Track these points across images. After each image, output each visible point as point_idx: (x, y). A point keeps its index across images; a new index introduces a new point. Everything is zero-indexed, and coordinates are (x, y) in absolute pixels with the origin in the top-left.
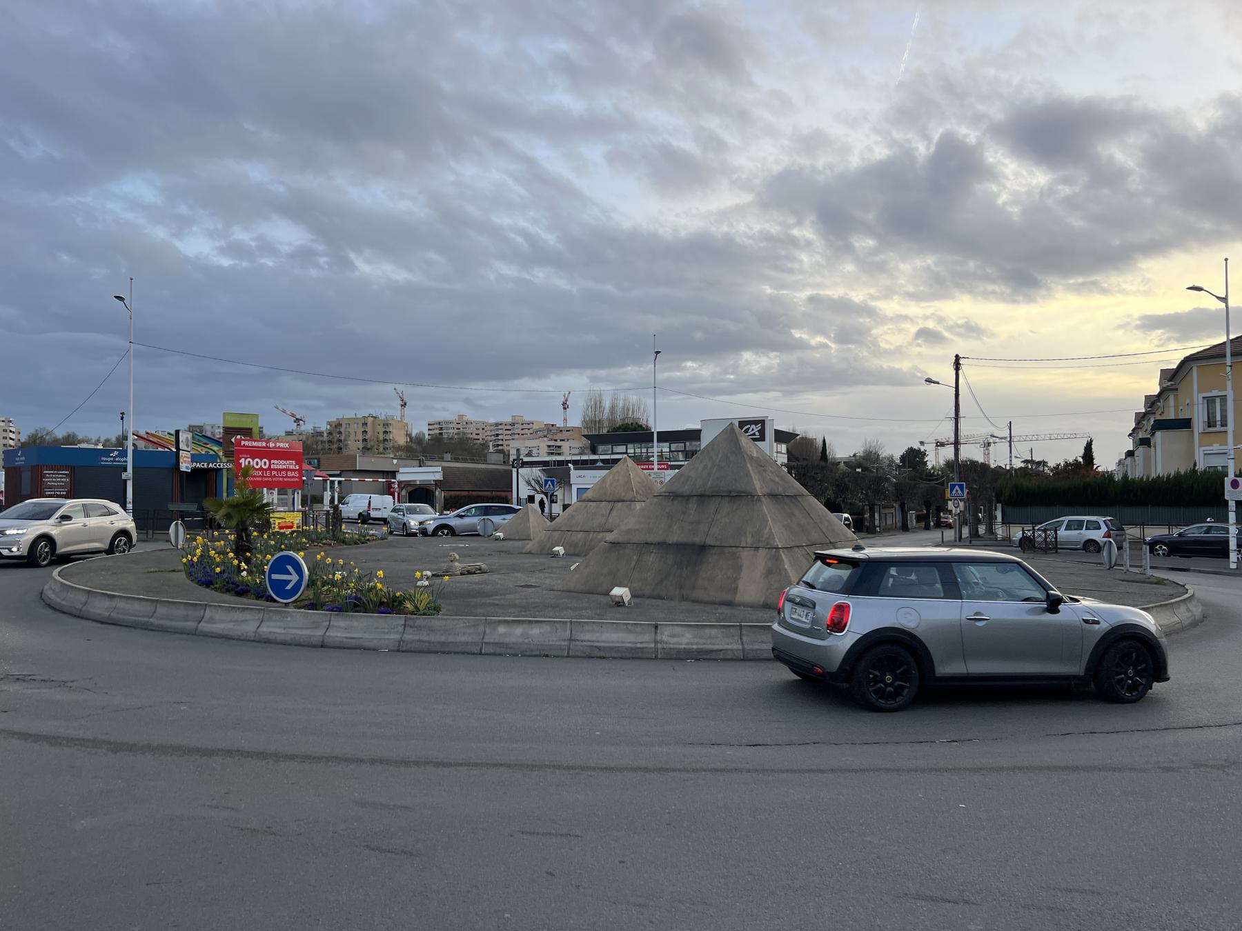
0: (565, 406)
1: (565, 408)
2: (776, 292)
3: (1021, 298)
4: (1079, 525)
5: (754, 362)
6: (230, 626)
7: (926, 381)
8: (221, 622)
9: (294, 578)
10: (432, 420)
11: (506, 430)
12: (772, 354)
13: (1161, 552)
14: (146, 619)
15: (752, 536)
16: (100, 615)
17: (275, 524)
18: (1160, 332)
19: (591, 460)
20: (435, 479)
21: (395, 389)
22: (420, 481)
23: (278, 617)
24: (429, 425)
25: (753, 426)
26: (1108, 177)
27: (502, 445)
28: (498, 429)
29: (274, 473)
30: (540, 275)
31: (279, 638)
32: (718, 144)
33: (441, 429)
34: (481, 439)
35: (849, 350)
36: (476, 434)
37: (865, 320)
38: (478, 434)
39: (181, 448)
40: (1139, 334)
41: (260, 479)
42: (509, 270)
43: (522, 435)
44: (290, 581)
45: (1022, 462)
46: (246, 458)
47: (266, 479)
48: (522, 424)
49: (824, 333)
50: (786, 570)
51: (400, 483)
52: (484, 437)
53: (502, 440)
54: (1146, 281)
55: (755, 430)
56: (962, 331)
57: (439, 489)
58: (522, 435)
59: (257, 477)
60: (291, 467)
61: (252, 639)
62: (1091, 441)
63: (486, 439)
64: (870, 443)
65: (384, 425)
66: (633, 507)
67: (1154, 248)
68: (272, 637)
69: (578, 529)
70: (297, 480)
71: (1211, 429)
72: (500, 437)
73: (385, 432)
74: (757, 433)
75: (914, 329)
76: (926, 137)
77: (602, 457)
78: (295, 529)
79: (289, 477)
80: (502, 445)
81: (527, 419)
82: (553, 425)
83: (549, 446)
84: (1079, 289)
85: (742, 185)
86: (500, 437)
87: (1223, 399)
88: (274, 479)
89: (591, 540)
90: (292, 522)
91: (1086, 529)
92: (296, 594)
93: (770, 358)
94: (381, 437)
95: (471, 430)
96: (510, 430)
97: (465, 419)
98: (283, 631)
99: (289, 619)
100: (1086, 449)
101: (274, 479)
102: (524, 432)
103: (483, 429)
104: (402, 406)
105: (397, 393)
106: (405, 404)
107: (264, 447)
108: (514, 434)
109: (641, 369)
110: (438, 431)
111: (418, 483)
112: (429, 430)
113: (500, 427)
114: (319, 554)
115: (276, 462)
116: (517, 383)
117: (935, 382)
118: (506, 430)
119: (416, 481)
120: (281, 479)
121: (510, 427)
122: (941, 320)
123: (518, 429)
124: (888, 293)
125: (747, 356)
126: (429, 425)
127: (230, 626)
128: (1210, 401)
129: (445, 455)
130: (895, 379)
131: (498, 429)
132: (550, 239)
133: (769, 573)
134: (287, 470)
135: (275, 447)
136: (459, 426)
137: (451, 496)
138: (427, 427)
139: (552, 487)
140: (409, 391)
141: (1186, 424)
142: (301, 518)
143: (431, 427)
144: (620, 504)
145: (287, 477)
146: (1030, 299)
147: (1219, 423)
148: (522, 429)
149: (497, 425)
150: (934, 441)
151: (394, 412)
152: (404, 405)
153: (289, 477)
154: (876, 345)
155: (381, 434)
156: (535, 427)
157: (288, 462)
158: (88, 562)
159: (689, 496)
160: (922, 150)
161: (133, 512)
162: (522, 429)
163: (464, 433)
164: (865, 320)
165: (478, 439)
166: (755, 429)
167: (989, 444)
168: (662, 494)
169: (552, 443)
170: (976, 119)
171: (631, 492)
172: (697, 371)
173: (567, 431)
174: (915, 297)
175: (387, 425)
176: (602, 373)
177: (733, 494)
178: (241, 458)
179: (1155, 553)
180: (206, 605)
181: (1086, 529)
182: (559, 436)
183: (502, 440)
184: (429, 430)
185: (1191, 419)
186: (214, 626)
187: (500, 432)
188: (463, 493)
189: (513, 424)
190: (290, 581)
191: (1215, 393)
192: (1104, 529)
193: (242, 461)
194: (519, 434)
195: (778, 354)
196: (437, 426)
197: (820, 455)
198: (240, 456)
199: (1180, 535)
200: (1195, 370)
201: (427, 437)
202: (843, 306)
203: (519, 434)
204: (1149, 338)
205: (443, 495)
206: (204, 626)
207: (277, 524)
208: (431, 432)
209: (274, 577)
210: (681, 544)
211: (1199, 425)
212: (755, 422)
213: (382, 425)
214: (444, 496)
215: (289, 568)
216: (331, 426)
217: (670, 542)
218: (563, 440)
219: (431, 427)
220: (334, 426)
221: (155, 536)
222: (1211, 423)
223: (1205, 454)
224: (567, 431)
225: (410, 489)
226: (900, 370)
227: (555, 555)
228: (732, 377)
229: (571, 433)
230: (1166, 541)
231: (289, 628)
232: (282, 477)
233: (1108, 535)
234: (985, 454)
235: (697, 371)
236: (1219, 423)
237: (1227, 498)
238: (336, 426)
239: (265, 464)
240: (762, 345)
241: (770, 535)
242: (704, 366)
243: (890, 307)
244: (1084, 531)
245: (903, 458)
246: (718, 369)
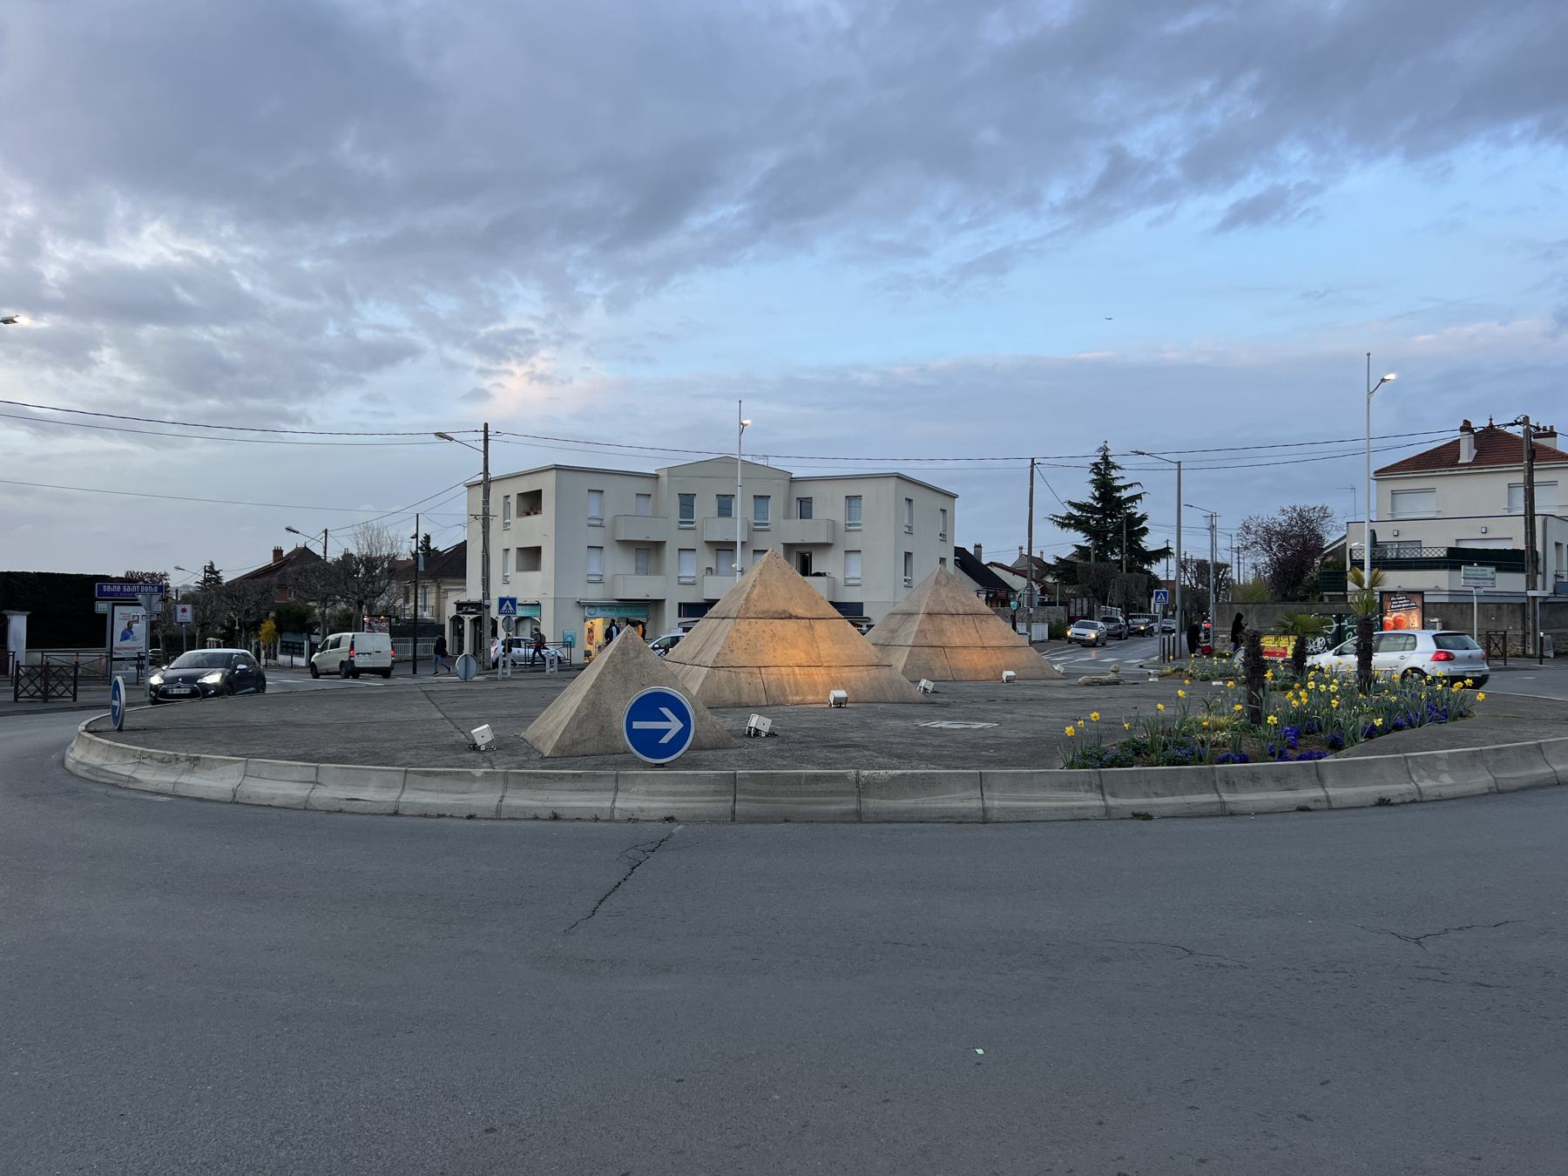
9: (675, 725)
209: (637, 725)
215: (666, 711)
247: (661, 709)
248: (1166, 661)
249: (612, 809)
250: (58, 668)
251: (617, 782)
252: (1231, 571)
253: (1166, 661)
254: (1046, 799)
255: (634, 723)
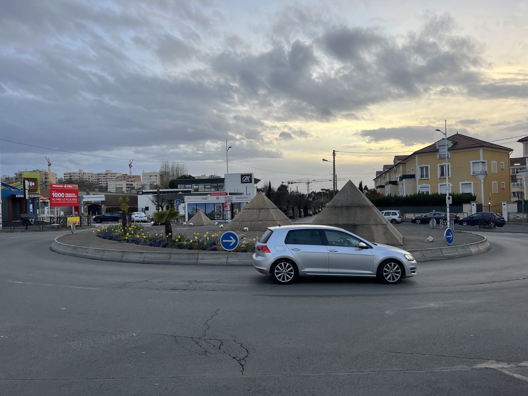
0: (130, 166)
1: (130, 167)
2: (219, 113)
3: (324, 120)
4: (388, 214)
5: (212, 145)
6: (213, 260)
7: (323, 160)
8: (208, 259)
9: (234, 241)
10: (66, 172)
11: (103, 177)
12: (219, 142)
13: (418, 223)
14: (167, 260)
15: (374, 221)
16: (137, 260)
17: (69, 222)
18: (368, 137)
19: (170, 191)
20: (101, 200)
21: (46, 157)
22: (94, 201)
23: (234, 256)
24: (64, 174)
25: (247, 177)
26: (361, 67)
27: (101, 184)
28: (99, 176)
29: (67, 199)
30: (107, 99)
31: (238, 264)
32: (195, 37)
33: (71, 176)
34: (90, 181)
35: (251, 142)
36: (88, 179)
37: (259, 129)
38: (89, 179)
39: (26, 188)
40: (361, 138)
41: (61, 202)
42: (90, 97)
43: (111, 179)
44: (232, 242)
45: (321, 190)
46: (55, 193)
47: (63, 202)
48: (111, 174)
49: (240, 133)
50: (391, 232)
51: (84, 202)
52: (92, 180)
53: (101, 181)
54: (371, 114)
55: (248, 178)
56: (298, 134)
57: (103, 205)
58: (111, 179)
59: (60, 201)
60: (74, 196)
61: (225, 265)
62: (361, 182)
63: (93, 181)
64: (266, 183)
65: (45, 174)
66: (269, 211)
67: (374, 100)
68: (235, 263)
69: (247, 220)
70: (76, 202)
71: (423, 178)
72: (100, 180)
73: (46, 178)
74: (249, 180)
75: (279, 132)
76: (288, 42)
77: (182, 190)
78: (77, 224)
79: (73, 201)
80: (101, 184)
81: (113, 172)
82: (126, 175)
83: (127, 184)
84: (347, 117)
85: (204, 58)
86: (100, 180)
87: (427, 168)
88: (67, 202)
89: (254, 225)
90: (76, 221)
91: (392, 215)
92: (226, 249)
93: (218, 144)
94: (44, 180)
95: (86, 177)
96: (105, 177)
97: (83, 171)
98: (239, 261)
99: (239, 256)
100: (360, 185)
101: (67, 202)
102: (112, 178)
103: (92, 176)
104: (49, 165)
105: (47, 159)
106: (51, 165)
107: (62, 188)
108: (107, 179)
109: (160, 147)
110: (69, 178)
111: (93, 202)
112: (64, 177)
113: (75, 175)
114: (205, 233)
115: (67, 194)
116: (96, 153)
117: (326, 161)
118: (103, 177)
119: (92, 201)
120: (70, 202)
121: (105, 176)
122: (290, 129)
123: (109, 176)
124: (267, 116)
125: (208, 143)
126: (64, 174)
127: (213, 260)
128: (422, 168)
129: (96, 189)
130: (269, 155)
131: (99, 176)
132: (111, 79)
133: (385, 233)
134: (72, 198)
135: (67, 187)
136: (79, 175)
137: (109, 208)
138: (63, 176)
139: (179, 203)
140: (52, 156)
141: (413, 176)
142: (79, 219)
143: (65, 176)
144: (263, 210)
145: (72, 201)
146: (328, 121)
147: (425, 176)
148: (111, 176)
149: (99, 174)
150: (287, 182)
151: (44, 168)
152: (50, 165)
153: (73, 201)
154: (262, 140)
155: (44, 179)
156: (118, 175)
157: (72, 194)
158: (463, 234)
159: (342, 207)
160: (287, 48)
161: (2, 219)
162: (111, 176)
163: (82, 178)
164: (259, 129)
165: (89, 181)
166: (248, 178)
167: (309, 183)
168: (330, 206)
169: (128, 183)
170: (311, 35)
171: (266, 205)
172: (185, 149)
173: (133, 177)
174: (279, 119)
175: (47, 174)
176: (140, 149)
177: (360, 206)
178: (53, 193)
179: (416, 223)
180: (199, 253)
181: (392, 215)
182: (130, 179)
183: (101, 181)
184: (64, 177)
185: (415, 175)
186: (206, 261)
187: (100, 178)
188: (115, 206)
189: (106, 174)
190: (232, 242)
191: (424, 165)
192: (398, 215)
193: (53, 194)
194: (109, 179)
195: (222, 142)
196: (69, 175)
197: (268, 188)
198: (52, 192)
199: (425, 216)
200: (417, 157)
201: (64, 180)
202: (249, 121)
203: (109, 179)
204: (365, 139)
205: (105, 207)
206: (200, 261)
207: (70, 222)
208: (65, 178)
209: (224, 241)
210: (345, 224)
211: (418, 177)
212: (248, 175)
213: (44, 174)
214: (106, 208)
215: (231, 237)
216: (16, 175)
217: (340, 224)
218: (132, 181)
219: (65, 176)
220: (18, 175)
221: (15, 230)
222: (422, 176)
223: (420, 187)
224: (133, 177)
225: (88, 205)
226: (272, 151)
227: (245, 231)
228: (201, 152)
229: (135, 178)
230: (420, 218)
231: (241, 259)
232: (70, 201)
233: (399, 217)
234: (307, 187)
235: (185, 149)
236: (425, 176)
237: (447, 203)
238: (19, 175)
239: (63, 195)
240: (214, 138)
241: (381, 220)
242: (189, 147)
243: (268, 123)
244: (391, 216)
245: (279, 189)
246: (195, 148)
247: (230, 237)
248: (217, 210)
249: (197, 262)
250: (365, 245)
251: (198, 255)
252: (365, 195)
253: (217, 210)
254: (196, 252)
255: (223, 240)
